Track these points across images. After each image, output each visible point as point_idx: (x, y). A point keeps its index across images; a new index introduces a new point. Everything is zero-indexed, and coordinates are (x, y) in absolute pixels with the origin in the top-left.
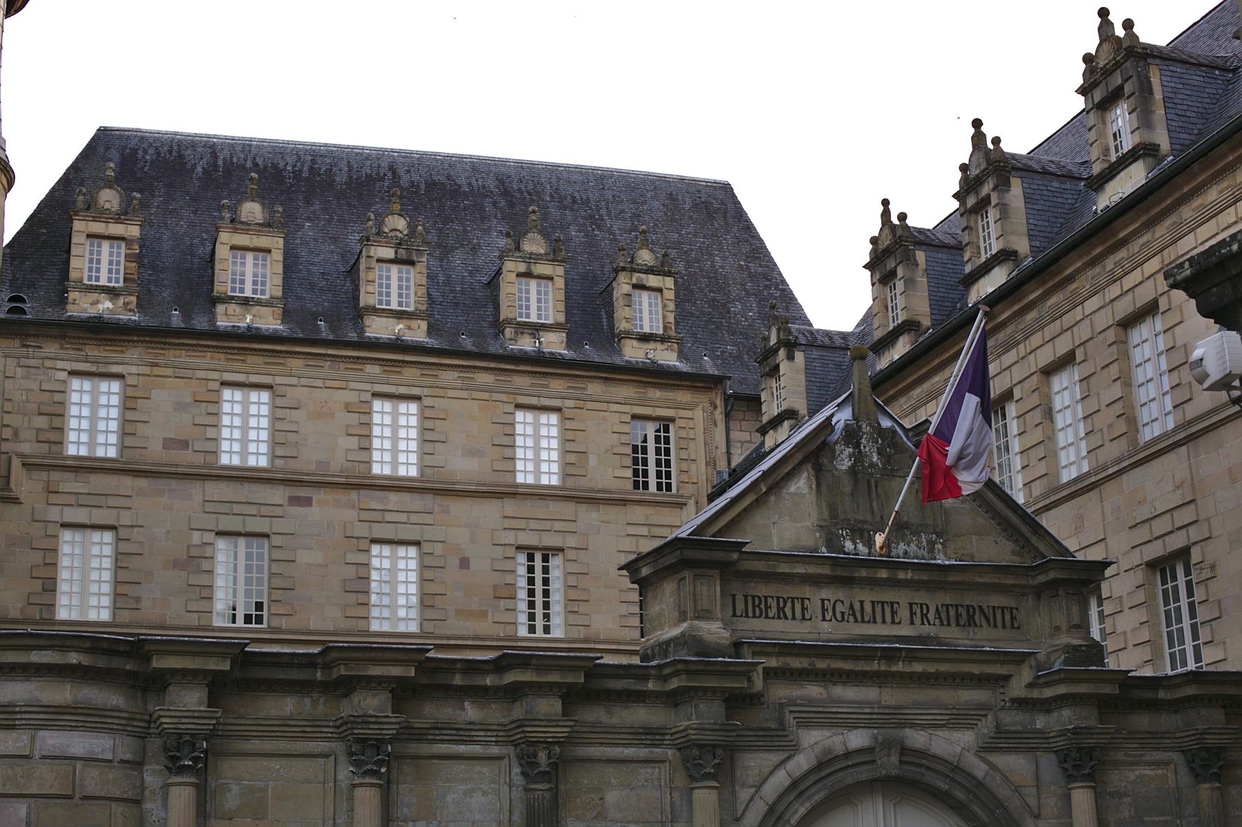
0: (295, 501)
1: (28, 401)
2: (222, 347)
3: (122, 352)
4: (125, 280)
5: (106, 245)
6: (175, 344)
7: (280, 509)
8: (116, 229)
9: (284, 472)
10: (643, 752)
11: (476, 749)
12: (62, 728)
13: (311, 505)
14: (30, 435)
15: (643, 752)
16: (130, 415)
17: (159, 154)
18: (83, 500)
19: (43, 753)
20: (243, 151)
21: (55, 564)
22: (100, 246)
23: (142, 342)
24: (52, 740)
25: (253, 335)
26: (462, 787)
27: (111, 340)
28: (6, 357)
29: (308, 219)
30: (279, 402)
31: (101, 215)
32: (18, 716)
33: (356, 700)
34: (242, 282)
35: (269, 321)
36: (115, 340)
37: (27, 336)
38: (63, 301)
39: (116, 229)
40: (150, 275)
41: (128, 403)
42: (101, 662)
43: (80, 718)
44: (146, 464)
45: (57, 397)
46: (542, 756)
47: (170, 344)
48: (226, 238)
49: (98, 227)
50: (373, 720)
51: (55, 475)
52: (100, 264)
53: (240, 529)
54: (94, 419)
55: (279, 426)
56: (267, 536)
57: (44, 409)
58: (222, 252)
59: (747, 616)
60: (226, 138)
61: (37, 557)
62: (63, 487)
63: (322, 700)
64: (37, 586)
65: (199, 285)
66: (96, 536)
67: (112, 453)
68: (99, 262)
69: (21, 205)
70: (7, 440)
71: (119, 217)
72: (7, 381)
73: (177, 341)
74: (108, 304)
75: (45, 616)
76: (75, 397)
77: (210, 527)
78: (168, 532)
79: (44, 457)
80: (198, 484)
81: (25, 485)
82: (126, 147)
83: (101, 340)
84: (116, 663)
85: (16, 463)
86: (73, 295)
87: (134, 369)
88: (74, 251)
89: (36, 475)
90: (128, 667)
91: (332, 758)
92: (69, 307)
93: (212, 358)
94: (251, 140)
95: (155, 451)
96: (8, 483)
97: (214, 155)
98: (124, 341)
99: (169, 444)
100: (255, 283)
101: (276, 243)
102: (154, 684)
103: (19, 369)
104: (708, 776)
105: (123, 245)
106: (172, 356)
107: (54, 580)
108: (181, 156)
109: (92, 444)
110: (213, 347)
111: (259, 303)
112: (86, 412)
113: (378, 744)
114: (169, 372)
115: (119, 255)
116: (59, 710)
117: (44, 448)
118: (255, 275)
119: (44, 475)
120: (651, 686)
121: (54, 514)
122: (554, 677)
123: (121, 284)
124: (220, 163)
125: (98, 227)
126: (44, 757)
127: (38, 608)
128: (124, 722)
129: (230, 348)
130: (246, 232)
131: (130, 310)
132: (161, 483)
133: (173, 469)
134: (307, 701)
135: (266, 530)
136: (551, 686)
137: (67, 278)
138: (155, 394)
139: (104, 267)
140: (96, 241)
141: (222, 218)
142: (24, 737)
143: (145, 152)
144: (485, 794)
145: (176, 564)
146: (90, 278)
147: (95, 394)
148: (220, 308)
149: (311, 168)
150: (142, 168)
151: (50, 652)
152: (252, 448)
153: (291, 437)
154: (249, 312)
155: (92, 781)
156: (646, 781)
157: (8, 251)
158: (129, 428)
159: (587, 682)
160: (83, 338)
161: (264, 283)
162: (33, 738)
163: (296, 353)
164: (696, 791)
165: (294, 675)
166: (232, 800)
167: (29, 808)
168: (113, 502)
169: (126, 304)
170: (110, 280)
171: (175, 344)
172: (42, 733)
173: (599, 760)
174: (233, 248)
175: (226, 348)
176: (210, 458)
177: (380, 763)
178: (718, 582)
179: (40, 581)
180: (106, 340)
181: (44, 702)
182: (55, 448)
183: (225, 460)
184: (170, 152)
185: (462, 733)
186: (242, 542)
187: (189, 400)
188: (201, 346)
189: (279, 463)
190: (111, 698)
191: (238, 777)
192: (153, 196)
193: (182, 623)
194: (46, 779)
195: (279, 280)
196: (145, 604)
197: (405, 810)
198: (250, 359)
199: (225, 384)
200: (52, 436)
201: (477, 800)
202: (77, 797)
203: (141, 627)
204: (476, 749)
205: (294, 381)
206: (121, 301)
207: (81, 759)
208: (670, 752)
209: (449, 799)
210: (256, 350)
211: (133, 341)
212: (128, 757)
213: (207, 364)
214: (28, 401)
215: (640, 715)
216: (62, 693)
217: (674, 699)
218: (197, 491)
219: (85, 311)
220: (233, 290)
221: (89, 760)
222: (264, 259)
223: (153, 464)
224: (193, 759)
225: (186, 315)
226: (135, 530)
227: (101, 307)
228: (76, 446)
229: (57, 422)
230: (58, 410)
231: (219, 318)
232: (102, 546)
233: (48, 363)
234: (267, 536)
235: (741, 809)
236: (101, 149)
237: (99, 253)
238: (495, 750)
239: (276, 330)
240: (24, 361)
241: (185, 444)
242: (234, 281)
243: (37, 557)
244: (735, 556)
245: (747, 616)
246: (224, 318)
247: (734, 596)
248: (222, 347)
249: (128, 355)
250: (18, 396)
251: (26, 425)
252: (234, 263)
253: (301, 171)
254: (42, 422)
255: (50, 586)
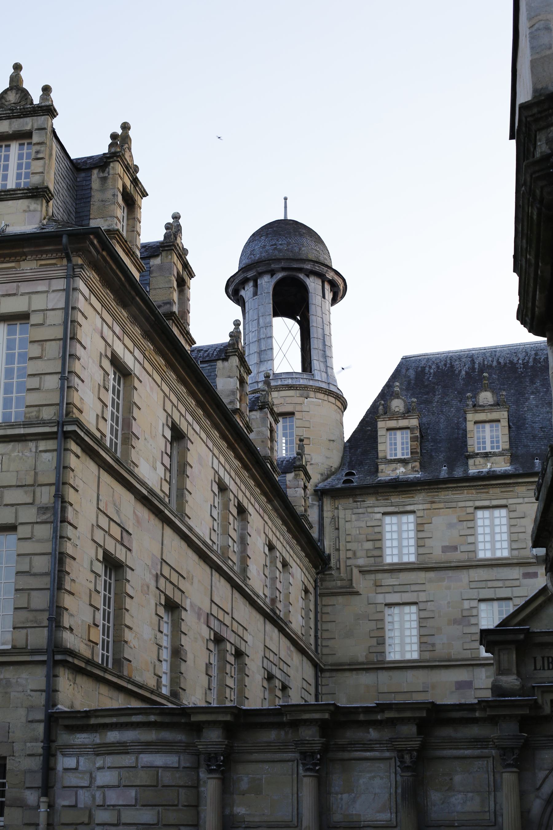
0: (527, 575)
1: (360, 534)
2: (473, 486)
3: (413, 497)
4: (412, 453)
5: (399, 433)
6: (443, 488)
7: (518, 581)
8: (403, 423)
9: (517, 559)
10: (477, 752)
11: (377, 754)
12: (151, 753)
13: (537, 577)
14: (363, 553)
15: (477, 752)
16: (421, 535)
17: (438, 367)
18: (397, 589)
19: (142, 765)
20: (491, 356)
21: (383, 628)
22: (395, 435)
23: (424, 489)
24: (146, 759)
25: (492, 476)
26: (368, 775)
27: (405, 491)
28: (345, 509)
29: (532, 393)
30: (513, 515)
31: (394, 416)
32: (129, 748)
33: (300, 732)
34: (484, 443)
35: (502, 465)
36: (408, 491)
37: (356, 495)
38: (377, 471)
39: (403, 423)
40: (432, 446)
41: (420, 527)
42: (167, 719)
43: (159, 747)
44: (432, 563)
45: (377, 529)
46: (407, 757)
47: (441, 488)
48: (471, 417)
49: (392, 424)
50: (306, 742)
51: (379, 576)
52: (396, 444)
53: (493, 596)
54: (400, 539)
55: (514, 530)
56: (510, 599)
57: (370, 537)
58: (470, 426)
59: (544, 669)
60: (480, 349)
61: (373, 625)
62: (385, 582)
63: (290, 731)
64: (374, 642)
65: (458, 448)
66: (407, 609)
67: (412, 559)
68: (395, 444)
69: (351, 422)
70: (350, 558)
71: (405, 415)
72: (347, 524)
73: (444, 486)
74: (402, 469)
75: (379, 659)
76: (388, 528)
77: (474, 597)
78: (449, 603)
79: (371, 566)
80: (465, 572)
81: (362, 583)
82: (418, 367)
83: (399, 492)
84: (176, 719)
85: (355, 571)
86: (381, 467)
87: (421, 507)
88: (380, 440)
89: (368, 576)
90: (183, 721)
91: (296, 762)
92: (379, 474)
93: (468, 493)
94: (496, 347)
95: (437, 555)
96: (352, 584)
97: (473, 362)
98: (413, 490)
99: (445, 549)
100: (492, 442)
101: (503, 415)
102: (197, 729)
103: (353, 516)
104: (509, 766)
105: (409, 431)
106: (444, 495)
107: (383, 637)
108: (452, 366)
109: (400, 554)
110: (467, 486)
111: (495, 454)
112: (395, 536)
113: (313, 754)
114: (442, 505)
115: (407, 438)
116: (148, 744)
117: (372, 560)
118: (492, 437)
119: (372, 576)
120: (477, 714)
121: (380, 599)
122: (408, 714)
123: (409, 456)
124: (476, 366)
125: (392, 424)
126: (142, 767)
127: (375, 654)
128: (184, 748)
129: (478, 486)
130: (483, 411)
131: (416, 471)
132: (442, 574)
133: (448, 565)
134: (283, 733)
135: (509, 595)
136: (409, 719)
137: (377, 458)
138: (434, 520)
139: (399, 447)
140: (393, 432)
141: (468, 405)
142: (133, 758)
143: (430, 367)
144: (382, 778)
145: (455, 622)
146: (391, 455)
147: (400, 524)
148: (471, 462)
149: (535, 359)
150: (429, 378)
151: (141, 716)
152: (498, 545)
153: (521, 535)
154: (488, 461)
155: (167, 778)
156: (479, 769)
157: (348, 444)
158: (421, 543)
159: (433, 717)
160: (388, 492)
161: (498, 442)
162: (137, 759)
163: (520, 483)
164: (504, 774)
165: (272, 719)
166: (244, 785)
167: (136, 792)
168: (414, 588)
169: (413, 468)
170: (403, 454)
171: (443, 488)
172: (141, 756)
173: (449, 758)
174: (476, 423)
175: (475, 486)
176: (471, 555)
177: (315, 765)
178: (514, 652)
179: (375, 639)
180: (402, 491)
181: (142, 740)
182: (378, 560)
183: (481, 555)
184: (445, 365)
185: (367, 746)
186: (496, 604)
187: (455, 521)
188: (460, 487)
189: (515, 553)
190: (179, 737)
191: (245, 775)
192: (435, 395)
193: (459, 657)
194: (143, 778)
195: (507, 439)
196: (438, 647)
197: (337, 788)
198: (491, 491)
199: (477, 508)
200: (376, 553)
201: (377, 782)
202: (160, 785)
203: (435, 661)
204: (377, 754)
205: (520, 500)
206: (410, 466)
207: (161, 767)
208: (493, 752)
209: (361, 781)
210: (494, 485)
211: (419, 490)
212: (188, 765)
213: (465, 498)
214: (360, 534)
215: (475, 731)
216: (151, 736)
217: (493, 720)
218: (465, 576)
219: (389, 475)
220: (479, 448)
221: (166, 768)
222: (497, 427)
223: (436, 563)
224: (216, 766)
225: (451, 469)
226: (429, 603)
227: (398, 471)
228: (391, 557)
229: (378, 544)
230: (378, 537)
231: (470, 467)
232: (410, 615)
233: (369, 510)
234: (510, 599)
235: (539, 783)
236: (404, 371)
237: (395, 439)
238: (387, 754)
239: (506, 470)
240: (356, 511)
241: (455, 548)
242: (479, 443)
243: (373, 625)
244: (522, 637)
245: (544, 669)
246: (474, 468)
247: (535, 659)
248: (473, 486)
249: (416, 499)
250: (354, 532)
251: (360, 548)
252: (478, 432)
253: (528, 362)
254: (369, 545)
255: (381, 641)
